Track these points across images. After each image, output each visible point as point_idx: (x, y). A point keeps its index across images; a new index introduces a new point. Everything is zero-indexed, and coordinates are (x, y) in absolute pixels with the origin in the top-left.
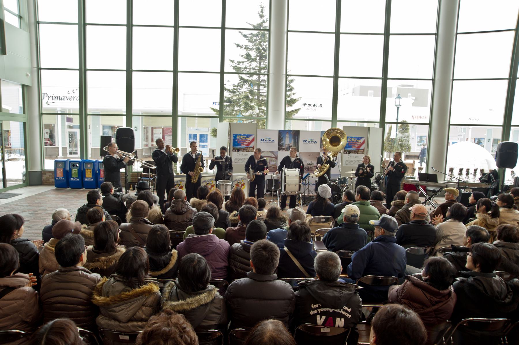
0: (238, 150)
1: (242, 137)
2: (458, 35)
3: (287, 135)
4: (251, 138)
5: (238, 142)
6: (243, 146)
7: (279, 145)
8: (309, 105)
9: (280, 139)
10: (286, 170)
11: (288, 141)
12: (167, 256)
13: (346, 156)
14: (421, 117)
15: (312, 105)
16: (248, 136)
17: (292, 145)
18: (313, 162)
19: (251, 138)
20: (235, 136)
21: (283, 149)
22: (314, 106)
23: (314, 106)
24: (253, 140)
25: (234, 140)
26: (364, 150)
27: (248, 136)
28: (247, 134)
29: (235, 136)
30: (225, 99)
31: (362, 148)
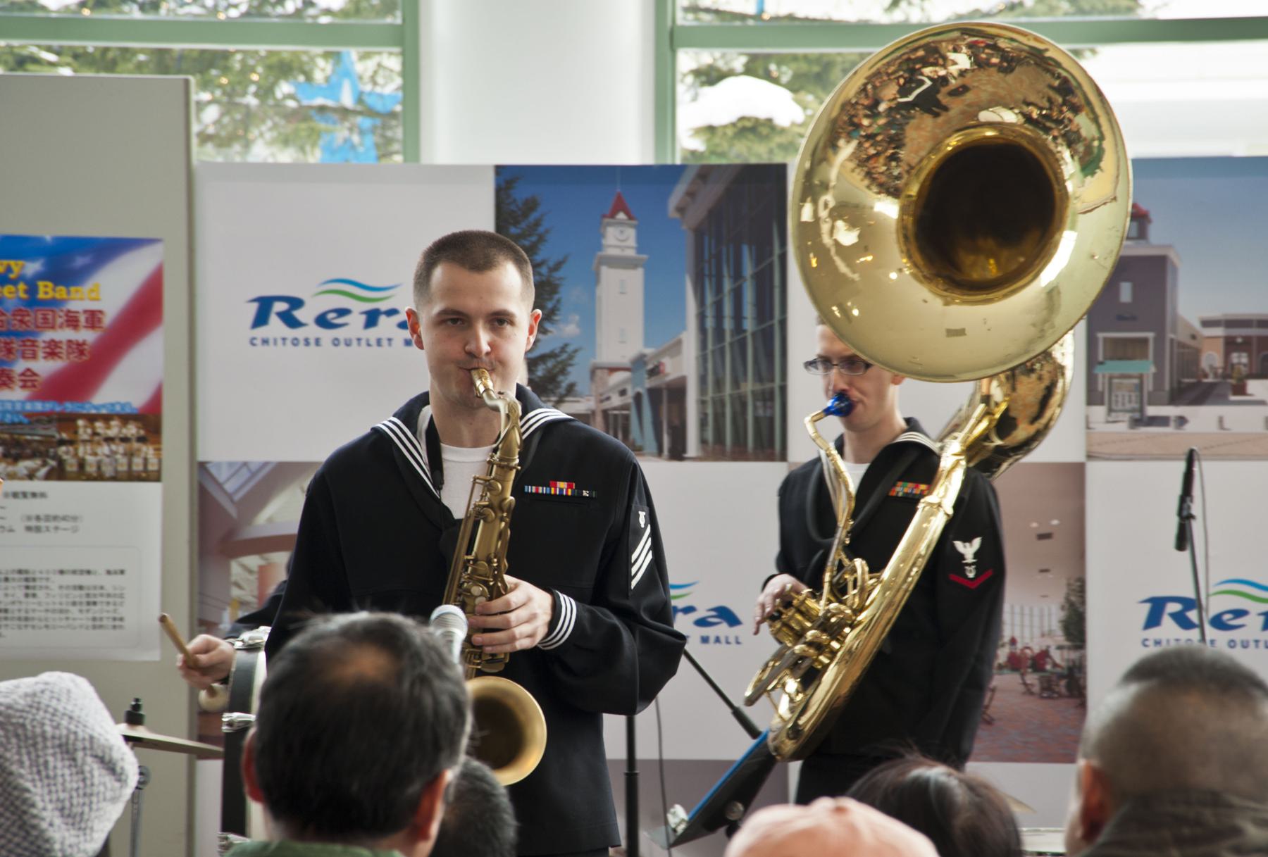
3: (620, 238)
16: (72, 259)
17: (685, 365)
19: (111, 290)
24: (144, 311)
26: (149, 421)
31: (122, 388)
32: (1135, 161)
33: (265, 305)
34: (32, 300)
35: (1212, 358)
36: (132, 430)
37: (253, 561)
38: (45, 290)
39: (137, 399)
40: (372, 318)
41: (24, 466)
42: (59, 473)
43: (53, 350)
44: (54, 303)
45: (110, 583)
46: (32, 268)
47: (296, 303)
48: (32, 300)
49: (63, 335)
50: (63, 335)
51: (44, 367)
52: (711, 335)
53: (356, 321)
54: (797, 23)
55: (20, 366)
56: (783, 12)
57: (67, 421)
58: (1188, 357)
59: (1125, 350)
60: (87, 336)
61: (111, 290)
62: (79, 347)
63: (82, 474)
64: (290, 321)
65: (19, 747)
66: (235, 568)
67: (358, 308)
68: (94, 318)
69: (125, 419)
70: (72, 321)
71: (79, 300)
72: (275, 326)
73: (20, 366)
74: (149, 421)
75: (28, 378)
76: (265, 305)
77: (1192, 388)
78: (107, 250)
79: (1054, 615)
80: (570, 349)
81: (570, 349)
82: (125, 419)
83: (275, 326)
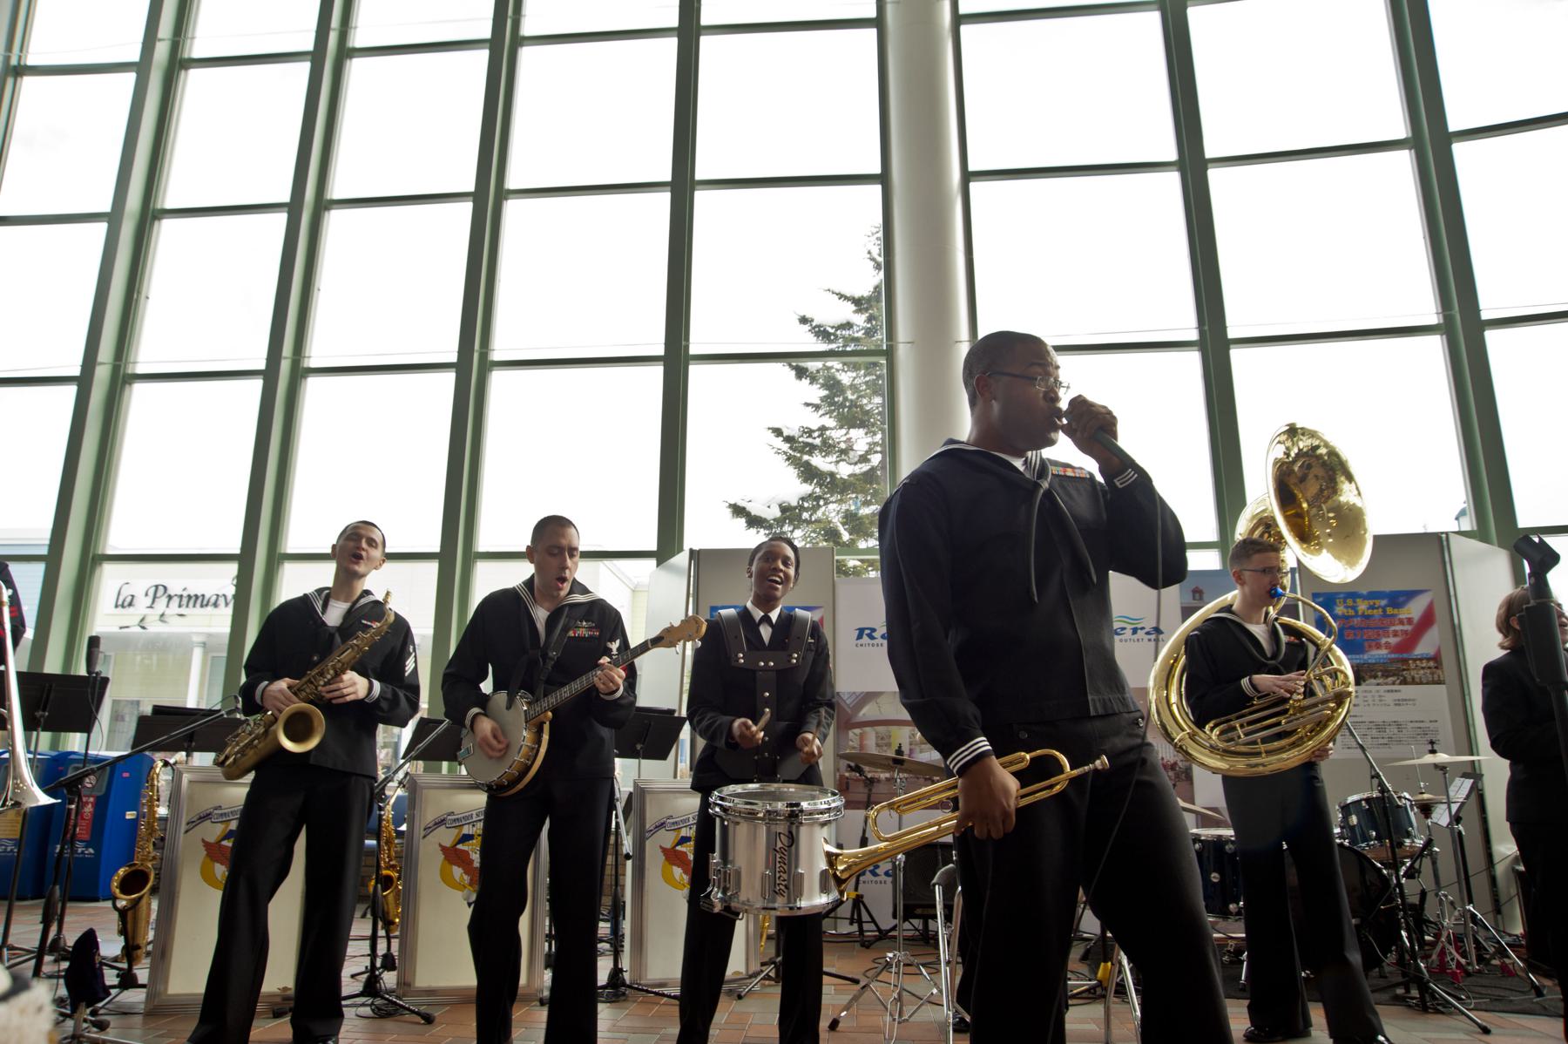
19: (1415, 609)
24: (1427, 620)
31: (1425, 647)
32: (1377, 538)
33: (861, 631)
34: (1385, 615)
36: (1432, 664)
37: (857, 731)
38: (1389, 610)
39: (1431, 652)
40: (1135, 631)
41: (1390, 679)
42: (1404, 682)
43: (1395, 634)
44: (1393, 616)
45: (1432, 726)
46: (1383, 602)
47: (874, 630)
48: (1385, 615)
49: (1399, 628)
50: (1399, 628)
51: (1393, 640)
53: (1128, 632)
55: (1384, 640)
57: (1405, 661)
60: (1408, 628)
61: (1415, 609)
62: (1405, 632)
63: (1414, 682)
64: (871, 637)
66: (851, 734)
67: (1129, 627)
68: (1410, 621)
69: (1429, 659)
70: (1401, 622)
71: (1404, 614)
72: (865, 639)
73: (1384, 640)
74: (1436, 659)
75: (1387, 645)
76: (861, 631)
78: (1411, 595)
82: (1429, 659)
83: (865, 639)
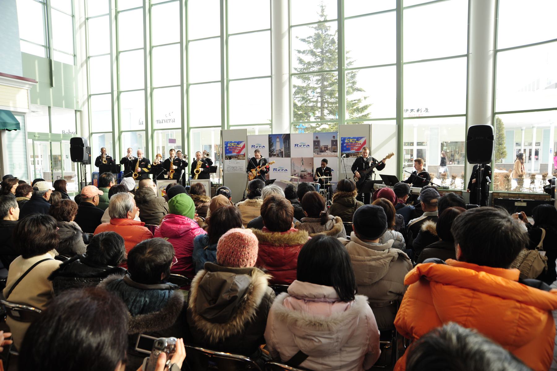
0: (230, 158)
1: (233, 144)
2: (466, 53)
3: (278, 140)
4: (241, 145)
5: (230, 150)
6: (353, 151)
7: (270, 150)
8: (412, 110)
9: (271, 145)
10: (352, 180)
11: (278, 146)
12: (126, 320)
13: (227, 162)
14: (166, 121)
15: (416, 110)
16: (239, 143)
17: (283, 150)
18: (306, 169)
19: (241, 145)
20: (227, 143)
21: (275, 155)
22: (418, 111)
23: (418, 111)
24: (244, 147)
25: (226, 148)
26: (244, 155)
27: (239, 143)
28: (237, 141)
29: (227, 143)
30: (320, 110)
31: (242, 153)
35: (323, 149)
52: (285, 148)
54: (461, 319)
56: (321, 163)
58: (321, 149)
59: (316, 148)
65: (79, 318)
74: (244, 155)
77: (322, 151)
78: (241, 142)
79: (311, 170)
80: (101, 343)
81: (101, 343)
